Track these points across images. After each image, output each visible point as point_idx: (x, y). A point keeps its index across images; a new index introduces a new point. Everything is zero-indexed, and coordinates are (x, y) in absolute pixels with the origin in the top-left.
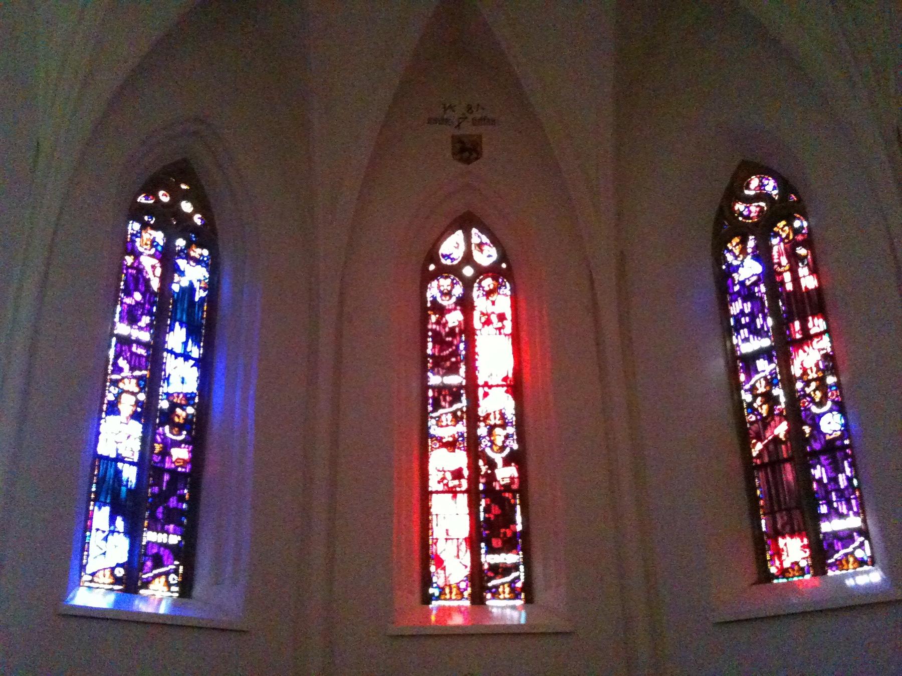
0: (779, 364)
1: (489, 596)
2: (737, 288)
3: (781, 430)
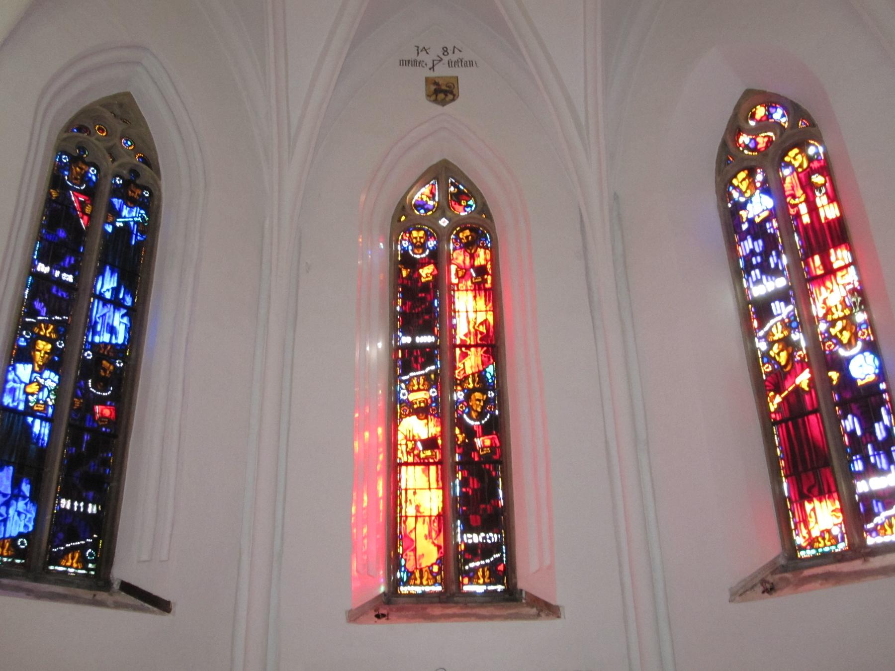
0: (797, 306)
1: (466, 580)
2: (745, 227)
3: (803, 379)
